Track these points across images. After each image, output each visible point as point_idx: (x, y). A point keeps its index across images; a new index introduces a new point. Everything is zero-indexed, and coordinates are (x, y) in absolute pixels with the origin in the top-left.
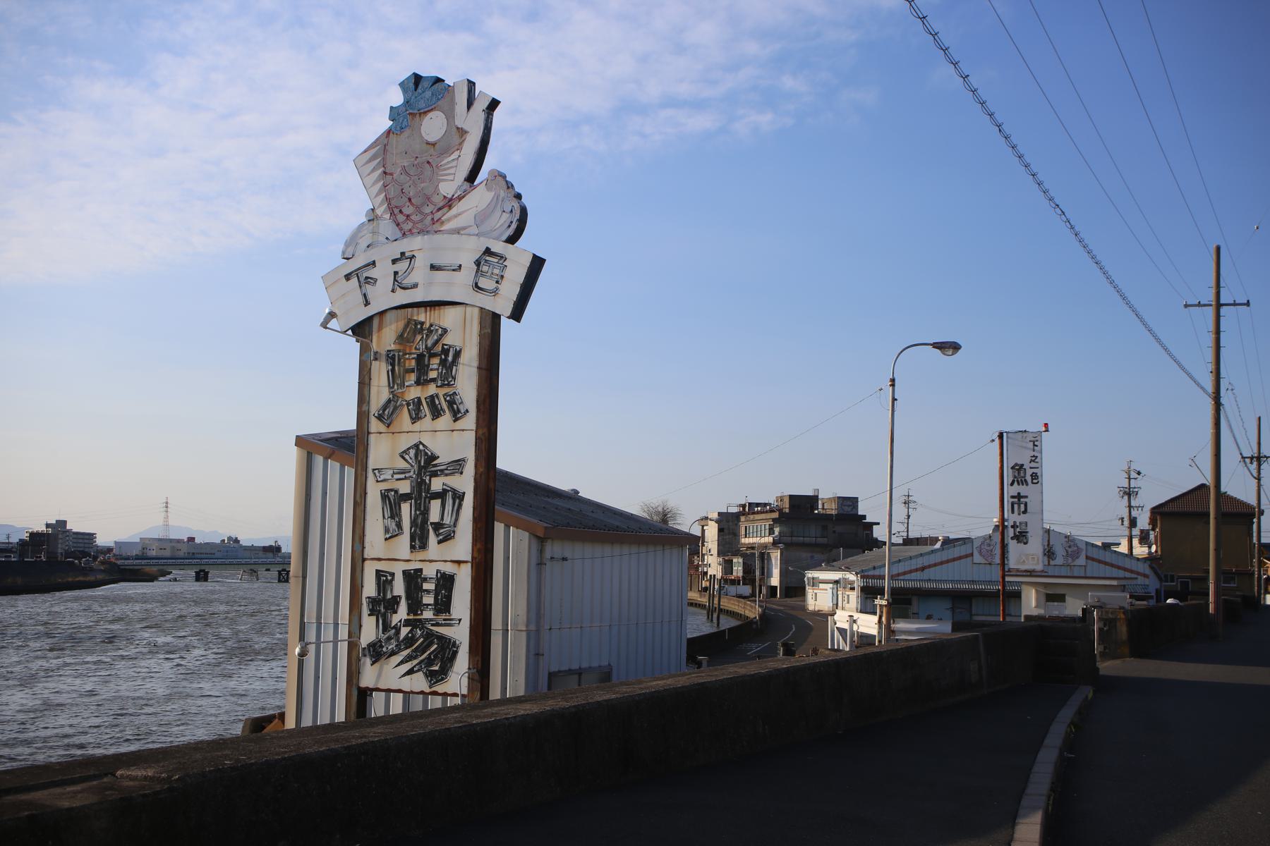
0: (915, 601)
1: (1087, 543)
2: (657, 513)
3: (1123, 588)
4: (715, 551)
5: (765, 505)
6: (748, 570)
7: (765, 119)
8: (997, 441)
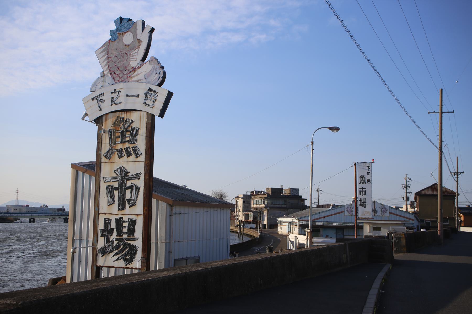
0: (321, 230)
1: (390, 207)
2: (218, 195)
3: (404, 225)
4: (241, 210)
5: (262, 192)
6: (255, 218)
7: (263, 37)
8: (354, 166)
